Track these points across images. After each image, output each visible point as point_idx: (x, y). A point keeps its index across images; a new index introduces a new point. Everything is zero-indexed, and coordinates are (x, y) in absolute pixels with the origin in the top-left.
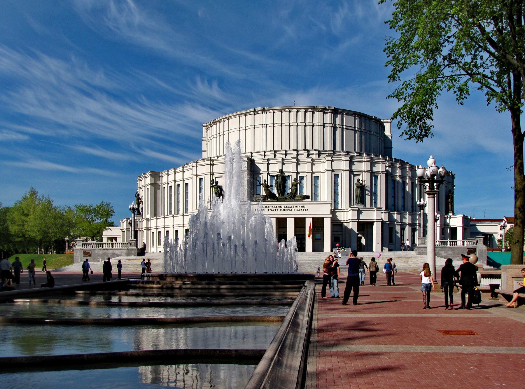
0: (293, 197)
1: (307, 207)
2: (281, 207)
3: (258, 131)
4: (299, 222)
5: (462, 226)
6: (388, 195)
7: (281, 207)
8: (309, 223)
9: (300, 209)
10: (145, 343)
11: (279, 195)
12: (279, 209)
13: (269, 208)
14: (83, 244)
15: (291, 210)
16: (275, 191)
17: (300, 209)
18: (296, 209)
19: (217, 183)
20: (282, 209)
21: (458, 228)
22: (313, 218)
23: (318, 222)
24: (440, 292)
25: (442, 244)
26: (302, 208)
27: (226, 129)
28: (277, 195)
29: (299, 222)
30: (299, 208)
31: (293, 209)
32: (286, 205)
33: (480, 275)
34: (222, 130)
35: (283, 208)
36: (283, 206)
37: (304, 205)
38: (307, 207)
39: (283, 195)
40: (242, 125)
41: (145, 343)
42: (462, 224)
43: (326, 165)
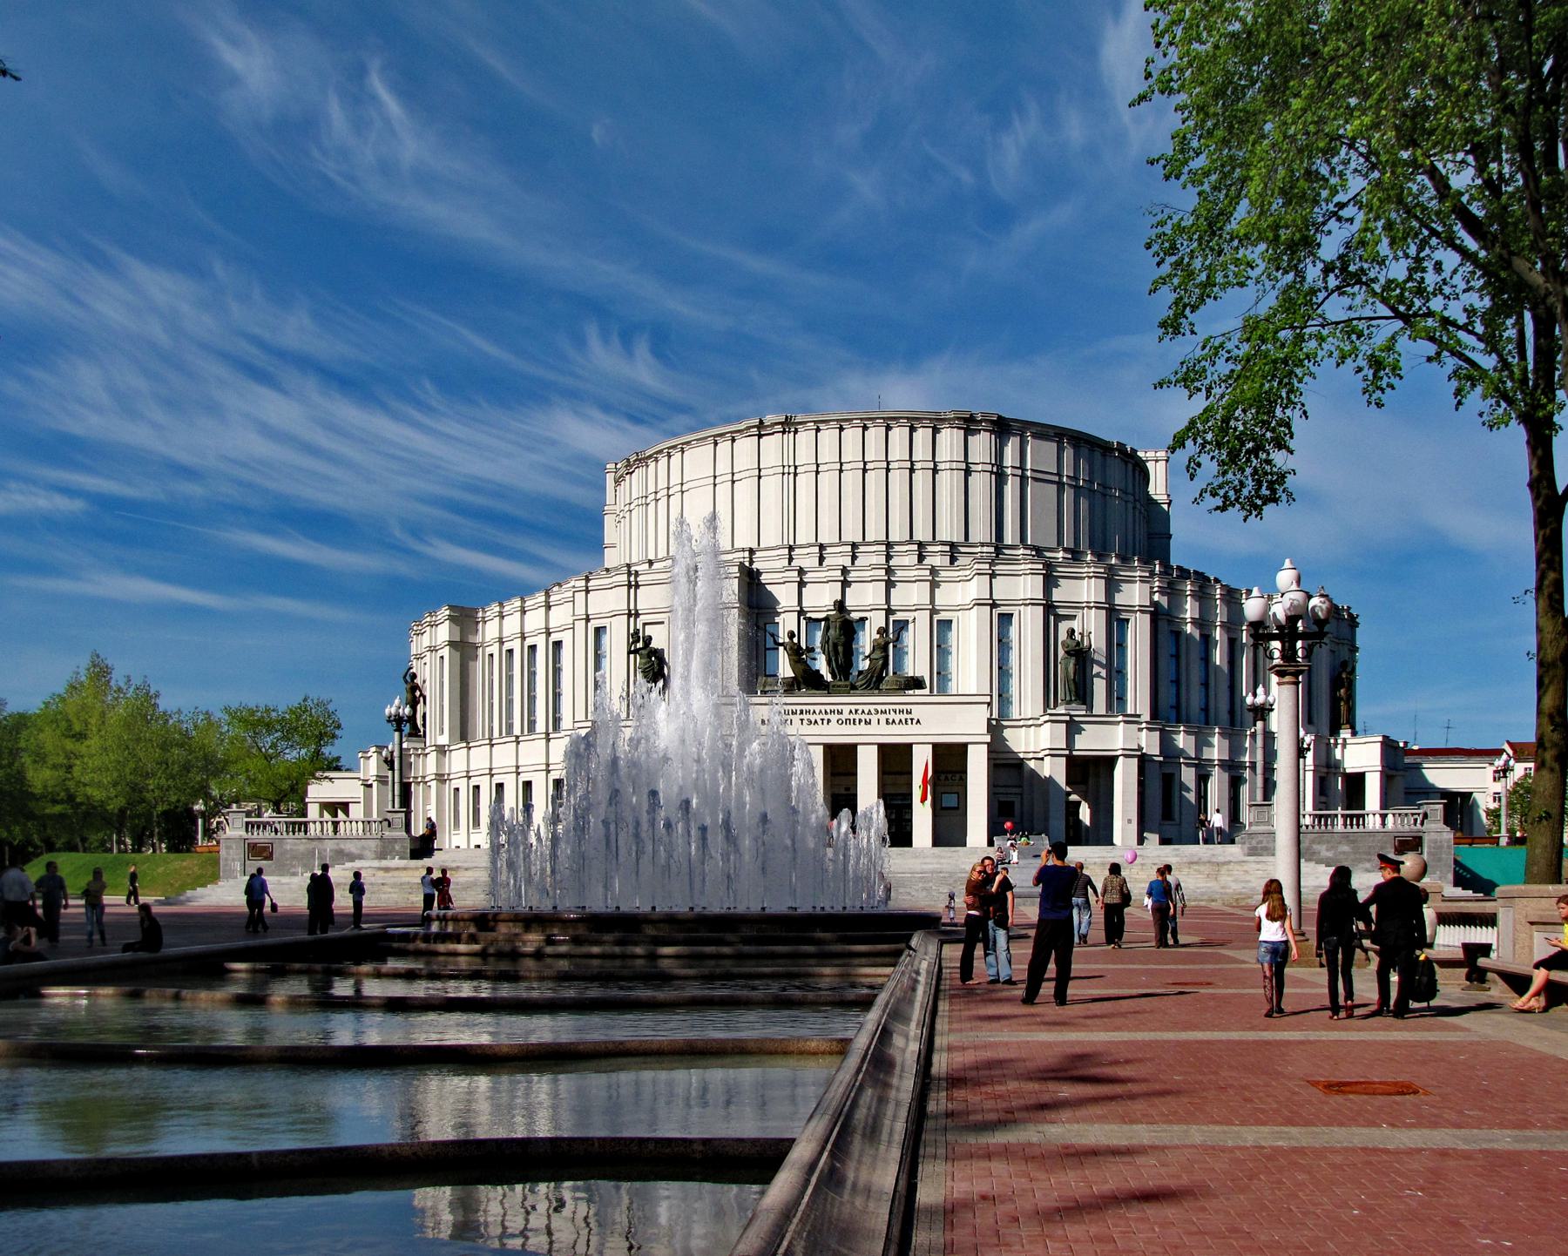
0: (874, 681)
1: (917, 712)
3: (771, 485)
4: (894, 759)
8: (922, 760)
9: (897, 718)
11: (834, 676)
12: (834, 718)
13: (804, 716)
15: (868, 723)
16: (821, 665)
17: (897, 718)
18: (883, 718)
19: (648, 640)
20: (843, 717)
21: (1368, 777)
22: (936, 746)
23: (950, 758)
25: (1320, 822)
26: (903, 717)
27: (676, 479)
28: (829, 678)
29: (894, 759)
30: (892, 716)
31: (874, 718)
32: (853, 708)
34: (662, 484)
35: (846, 715)
36: (846, 709)
37: (909, 707)
38: (917, 712)
39: (845, 678)
40: (723, 467)
43: (975, 588)
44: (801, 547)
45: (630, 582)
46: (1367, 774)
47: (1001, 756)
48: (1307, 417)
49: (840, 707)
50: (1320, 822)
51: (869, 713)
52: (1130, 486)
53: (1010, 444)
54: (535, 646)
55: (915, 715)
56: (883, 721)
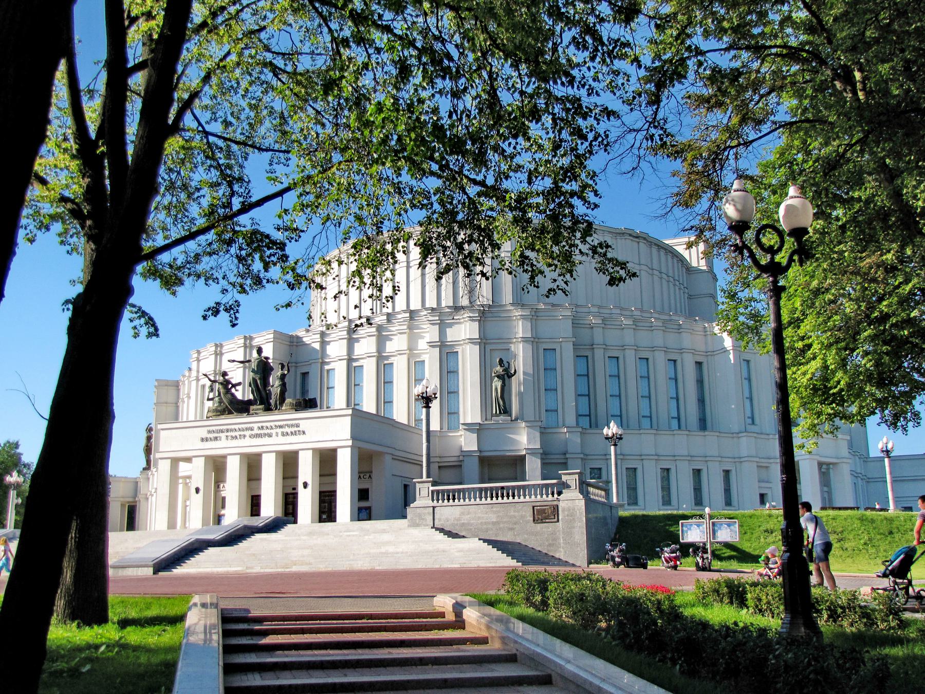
1: (304, 425)
2: (252, 429)
5: (350, 443)
6: (596, 358)
7: (252, 429)
9: (288, 430)
10: (100, 631)
12: (248, 433)
13: (229, 434)
14: (433, 492)
15: (270, 436)
17: (288, 430)
18: (279, 431)
20: (253, 432)
21: (302, 455)
22: (278, 453)
24: (556, 578)
25: (481, 494)
26: (293, 429)
31: (273, 432)
32: (260, 425)
33: (213, 618)
35: (256, 431)
36: (256, 426)
37: (297, 422)
41: (100, 631)
42: (348, 435)
44: (399, 313)
45: (245, 344)
46: (339, 451)
47: (445, 460)
48: (155, 333)
49: (297, 422)
50: (481, 494)
51: (272, 428)
52: (663, 265)
53: (667, 242)
54: (308, 373)
55: (301, 429)
56: (280, 434)
